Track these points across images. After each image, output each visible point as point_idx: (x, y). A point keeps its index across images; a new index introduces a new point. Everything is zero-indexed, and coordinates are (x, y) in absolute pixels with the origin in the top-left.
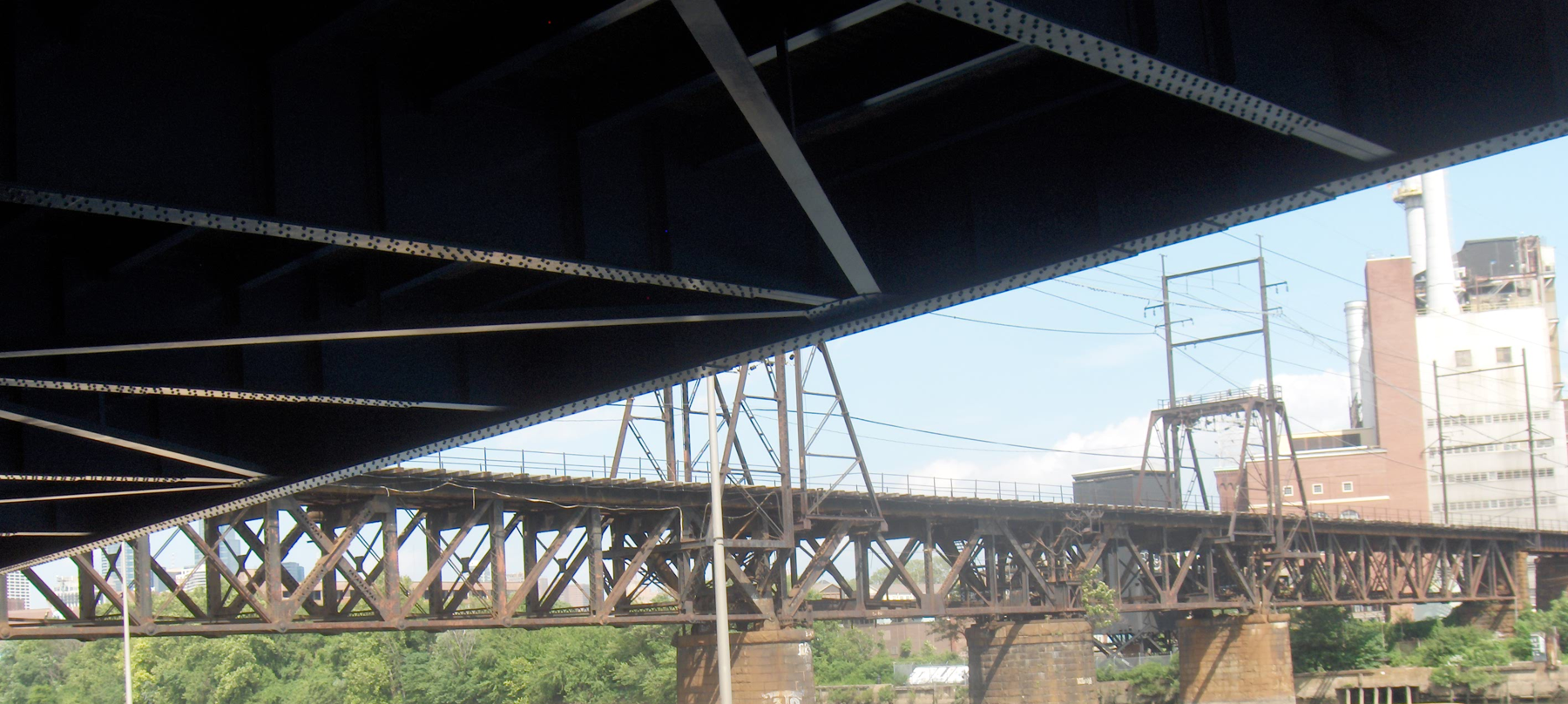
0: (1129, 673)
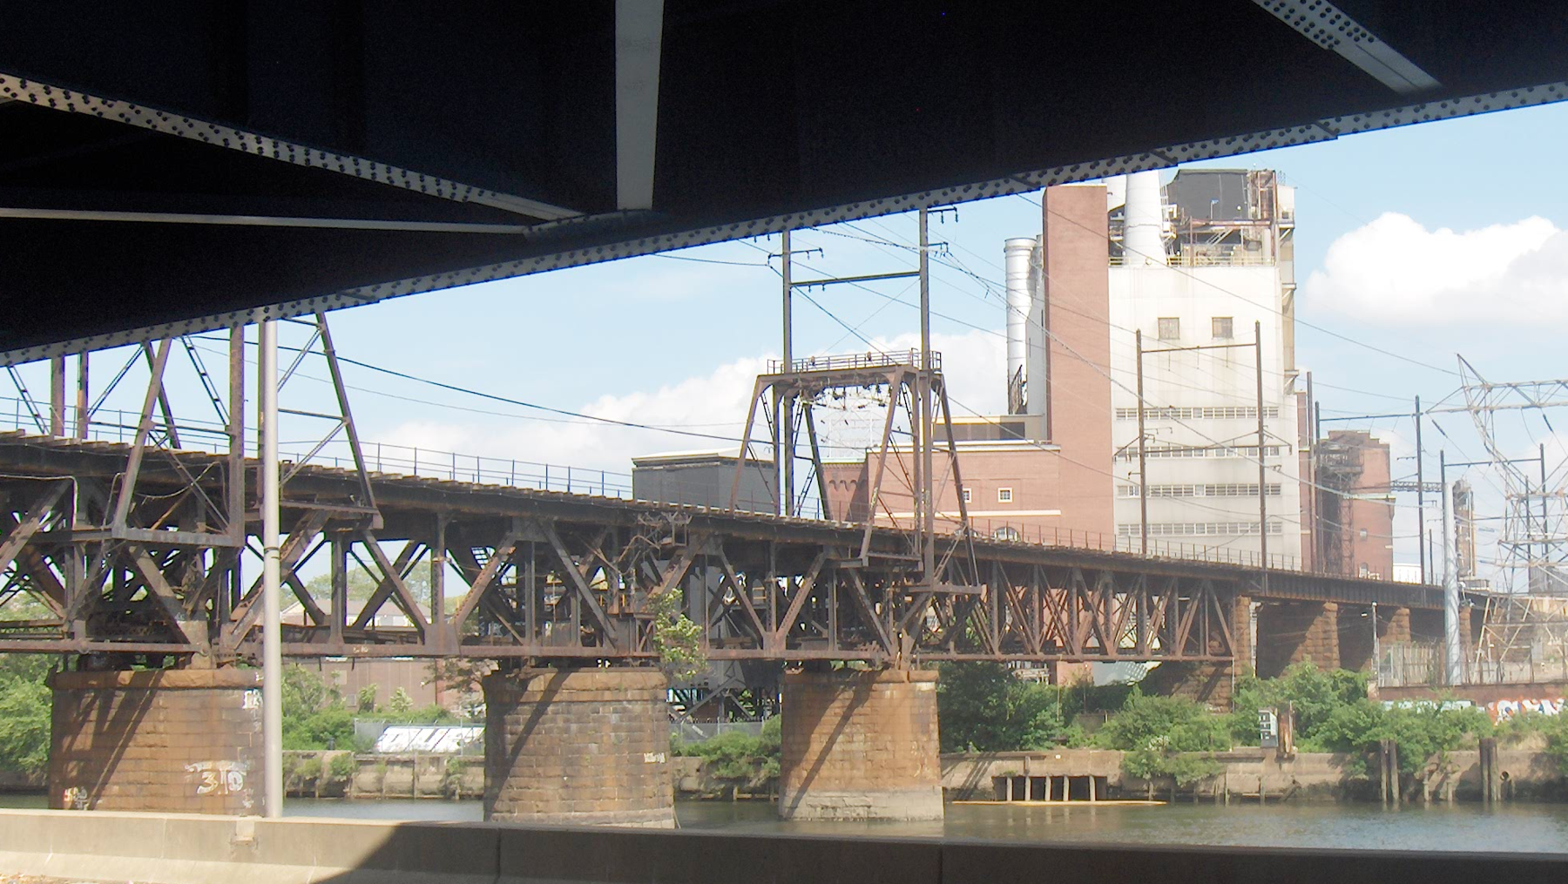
0: (702, 747)
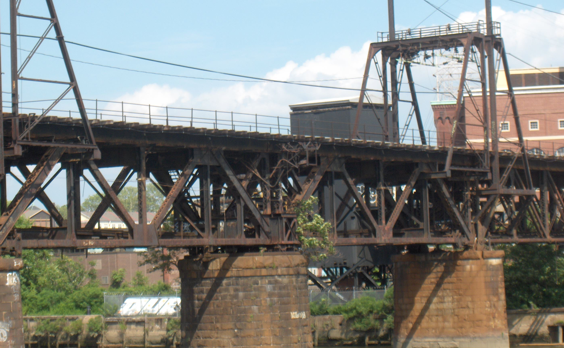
0: (343, 308)
